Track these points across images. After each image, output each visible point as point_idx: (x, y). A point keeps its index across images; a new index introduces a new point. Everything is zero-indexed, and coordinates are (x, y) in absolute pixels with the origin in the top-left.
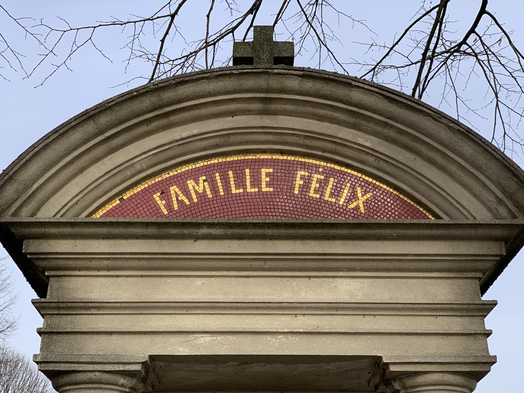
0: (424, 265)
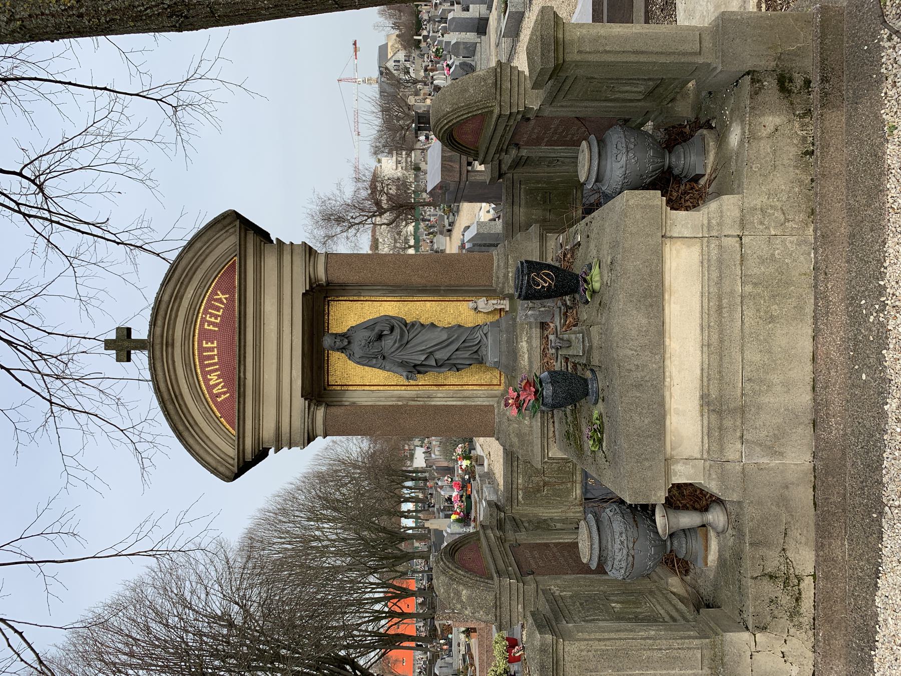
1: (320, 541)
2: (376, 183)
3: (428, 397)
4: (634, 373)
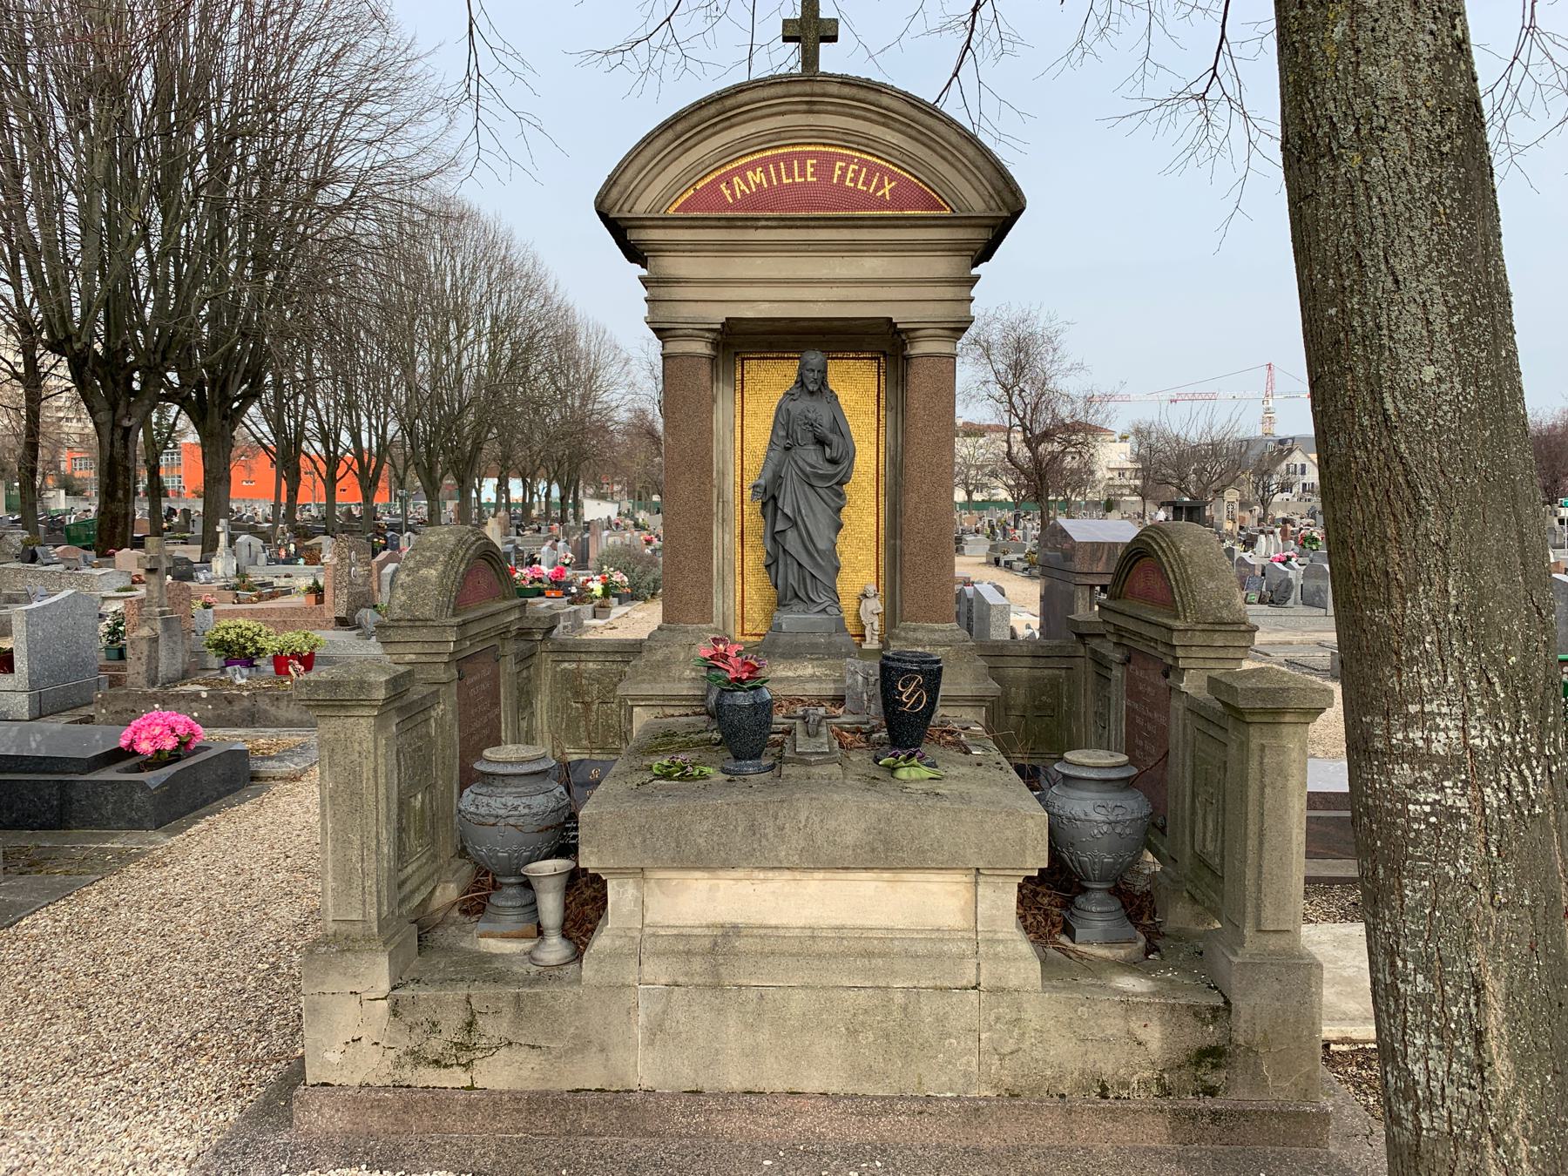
0: (930, 247)
1: (458, 339)
2: (1081, 432)
3: (723, 520)
4: (771, 824)
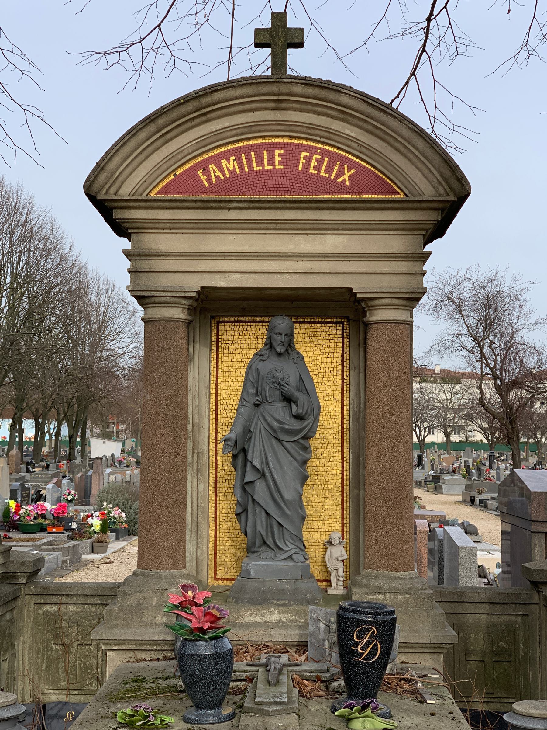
0: (385, 227)
3: (198, 470)
